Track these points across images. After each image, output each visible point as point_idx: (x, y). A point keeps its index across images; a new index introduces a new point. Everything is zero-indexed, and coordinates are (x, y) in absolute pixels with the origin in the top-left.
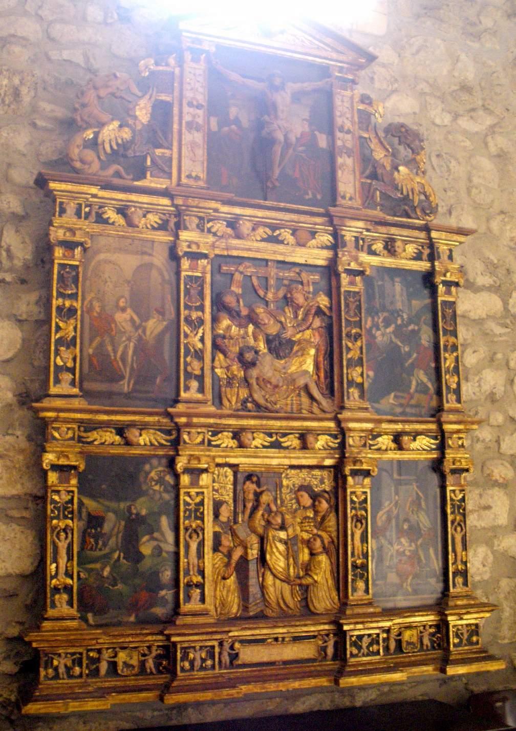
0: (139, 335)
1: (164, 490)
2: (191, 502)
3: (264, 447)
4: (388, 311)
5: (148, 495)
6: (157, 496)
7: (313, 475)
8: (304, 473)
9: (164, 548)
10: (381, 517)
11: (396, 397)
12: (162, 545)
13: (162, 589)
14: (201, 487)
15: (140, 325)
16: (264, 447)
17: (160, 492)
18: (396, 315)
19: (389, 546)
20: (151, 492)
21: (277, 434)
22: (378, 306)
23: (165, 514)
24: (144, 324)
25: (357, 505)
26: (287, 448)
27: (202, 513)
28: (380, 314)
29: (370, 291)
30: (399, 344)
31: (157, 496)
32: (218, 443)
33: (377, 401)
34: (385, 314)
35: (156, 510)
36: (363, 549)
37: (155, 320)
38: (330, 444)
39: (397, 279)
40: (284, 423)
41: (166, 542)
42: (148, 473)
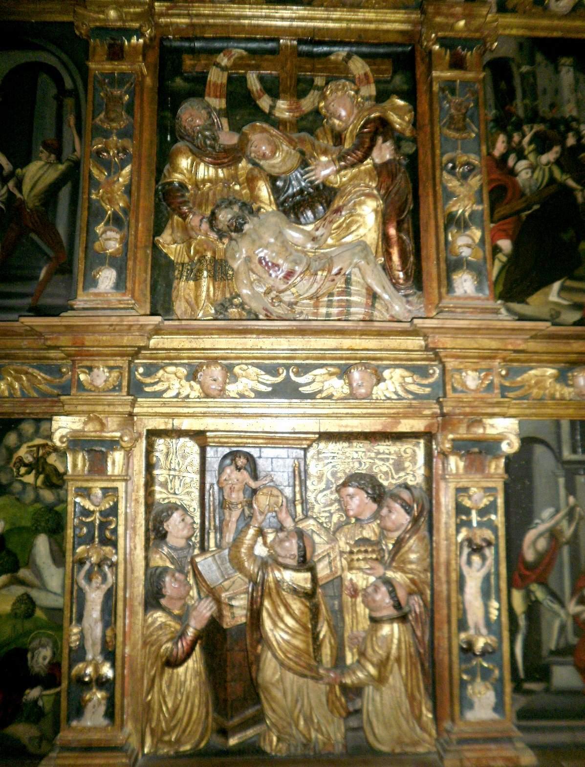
0: (8, 190)
1: (44, 483)
2: (92, 508)
3: (259, 394)
4: (543, 120)
5: (11, 493)
6: (30, 495)
7: (378, 453)
8: (359, 448)
9: (38, 603)
10: (534, 543)
11: (563, 289)
12: (34, 594)
13: (32, 687)
14: (111, 479)
15: (12, 174)
16: (259, 394)
17: (36, 488)
18: (562, 128)
19: (556, 607)
20: (17, 487)
21: (287, 367)
22: (521, 112)
23: (44, 531)
24: (19, 171)
25: (474, 517)
26: (312, 396)
27: (115, 531)
28: (526, 128)
29: (503, 85)
30: (571, 183)
31: (30, 495)
32: (157, 388)
33: (522, 299)
34: (537, 127)
35: (27, 522)
36: (487, 613)
37: (39, 164)
38: (413, 388)
39: (566, 61)
40: (297, 342)
41: (43, 587)
42: (11, 451)
